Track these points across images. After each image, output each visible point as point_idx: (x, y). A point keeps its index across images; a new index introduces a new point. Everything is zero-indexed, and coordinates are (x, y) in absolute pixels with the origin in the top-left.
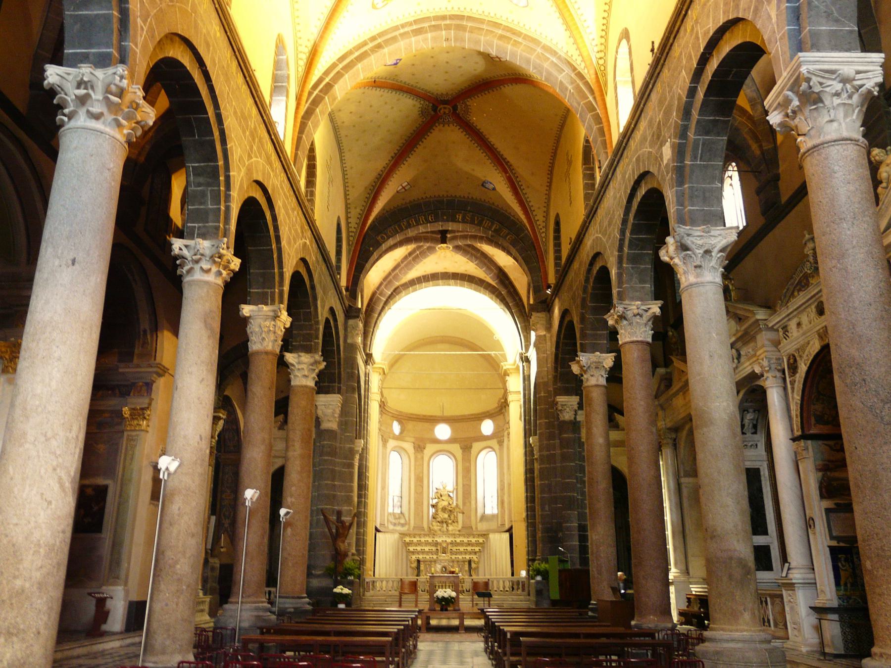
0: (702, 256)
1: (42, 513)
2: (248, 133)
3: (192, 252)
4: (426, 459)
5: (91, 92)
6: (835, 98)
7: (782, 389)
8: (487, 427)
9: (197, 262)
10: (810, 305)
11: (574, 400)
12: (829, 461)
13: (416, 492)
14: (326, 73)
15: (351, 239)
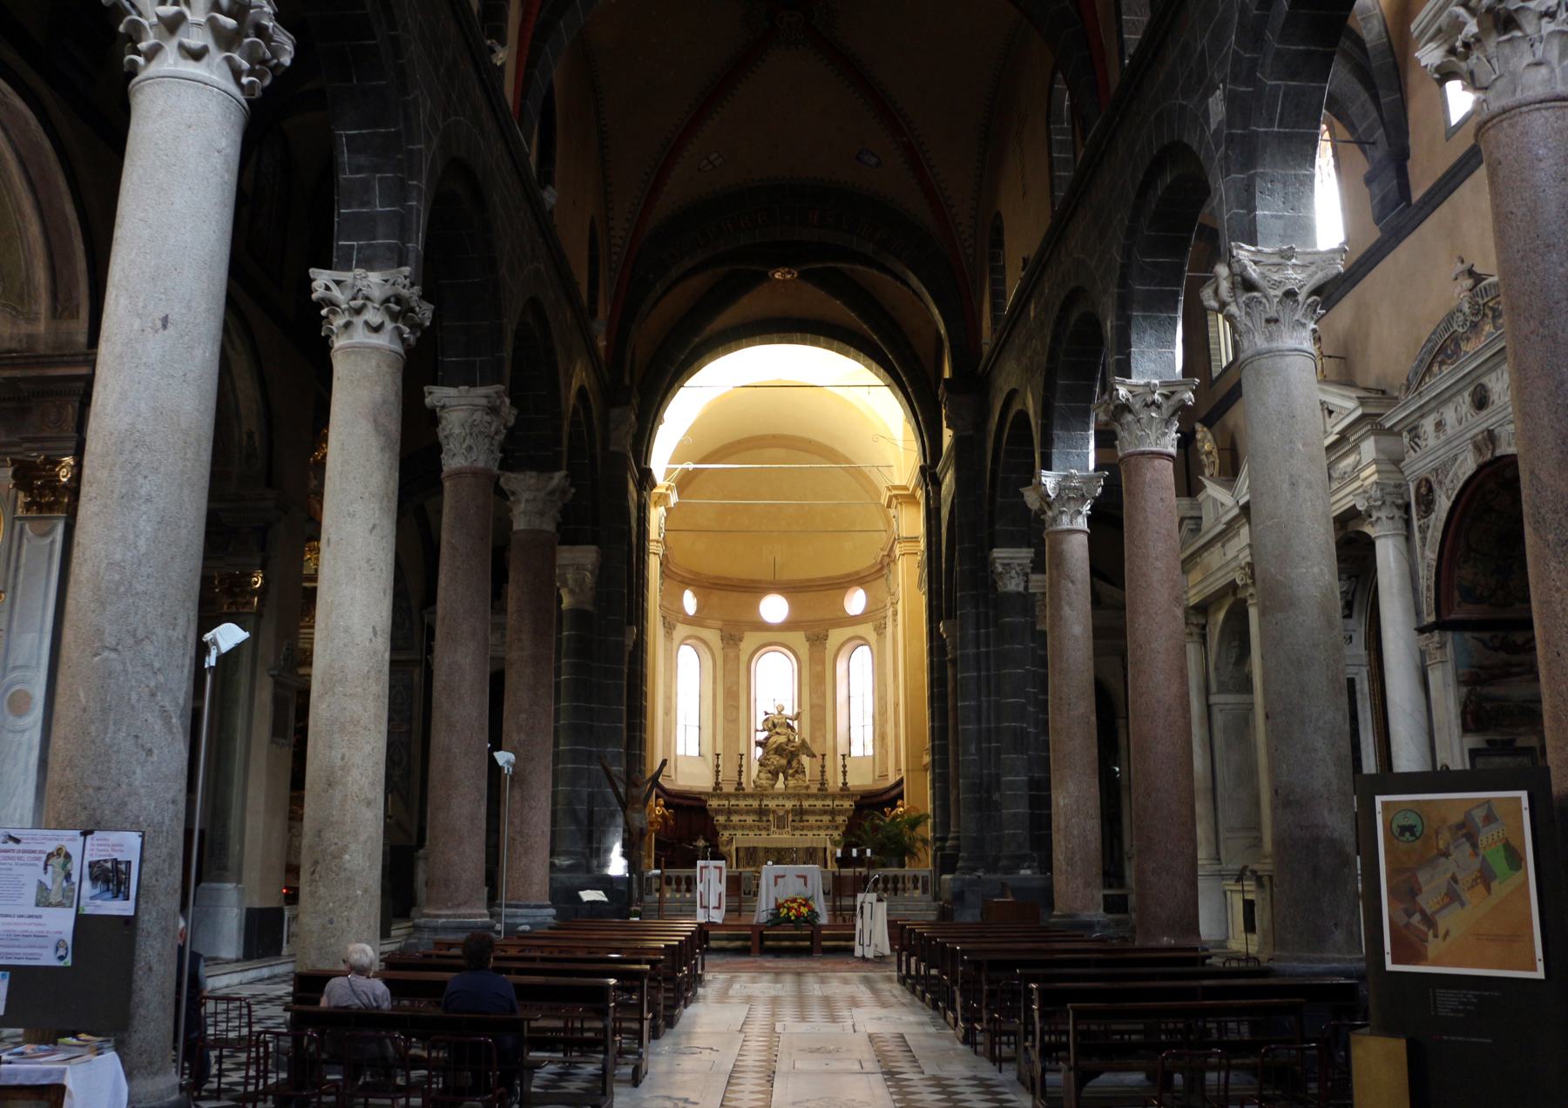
0: (1280, 302)
1: (138, 771)
3: (349, 294)
4: (744, 658)
5: (184, 9)
6: (1546, 20)
7: (1402, 540)
8: (856, 602)
9: (358, 311)
10: (1459, 392)
11: (1025, 554)
12: (1481, 667)
14: (989, 360)
15: (615, 258)
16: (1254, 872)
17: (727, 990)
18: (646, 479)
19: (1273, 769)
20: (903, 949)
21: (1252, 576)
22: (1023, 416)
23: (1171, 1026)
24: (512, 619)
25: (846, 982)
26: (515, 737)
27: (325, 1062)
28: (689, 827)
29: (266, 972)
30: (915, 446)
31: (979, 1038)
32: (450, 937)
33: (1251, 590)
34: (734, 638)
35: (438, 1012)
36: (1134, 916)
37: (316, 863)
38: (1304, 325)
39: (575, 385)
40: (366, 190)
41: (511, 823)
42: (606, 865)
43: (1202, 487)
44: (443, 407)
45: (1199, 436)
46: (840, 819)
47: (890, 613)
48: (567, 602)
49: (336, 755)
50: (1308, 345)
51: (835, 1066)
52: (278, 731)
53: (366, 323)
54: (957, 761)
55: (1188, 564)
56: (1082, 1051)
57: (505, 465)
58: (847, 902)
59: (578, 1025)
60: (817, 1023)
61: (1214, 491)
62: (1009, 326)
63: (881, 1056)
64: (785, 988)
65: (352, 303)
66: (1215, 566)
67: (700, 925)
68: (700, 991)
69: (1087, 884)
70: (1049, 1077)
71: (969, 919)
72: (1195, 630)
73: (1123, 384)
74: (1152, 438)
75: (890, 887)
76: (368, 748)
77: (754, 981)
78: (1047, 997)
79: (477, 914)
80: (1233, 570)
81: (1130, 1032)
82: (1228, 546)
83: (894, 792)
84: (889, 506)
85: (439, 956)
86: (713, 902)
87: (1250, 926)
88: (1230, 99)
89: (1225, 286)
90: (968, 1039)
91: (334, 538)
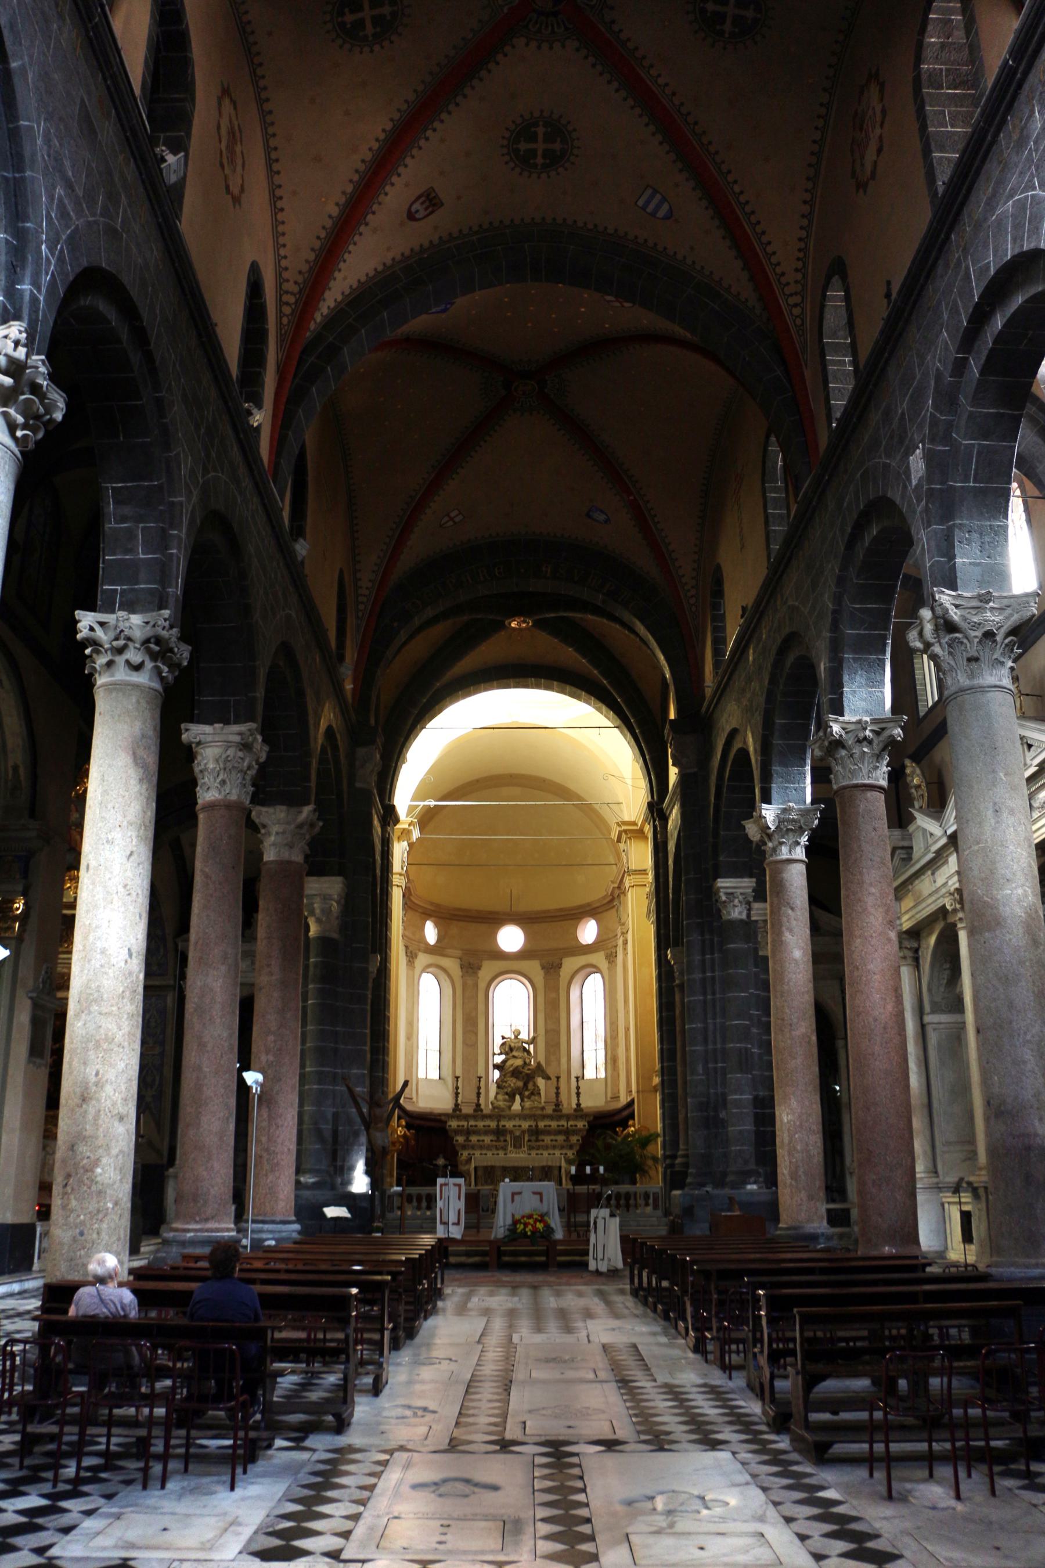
0: (980, 642)
2: (203, 430)
3: (112, 634)
4: (482, 985)
8: (588, 932)
9: (120, 651)
11: (747, 884)
13: (465, 1043)
15: (361, 607)
16: (969, 1184)
17: (466, 1303)
18: (390, 815)
19: (985, 1082)
20: (635, 1261)
21: (961, 901)
22: (744, 752)
23: (894, 1332)
24: (261, 945)
25: (580, 1294)
26: (263, 1058)
27: (71, 1372)
28: (427, 1147)
29: (16, 1287)
30: (643, 784)
31: (710, 1347)
32: (199, 1251)
33: (960, 915)
34: (472, 969)
35: (185, 1321)
36: (856, 1229)
37: (69, 1176)
38: (1002, 663)
39: (323, 725)
40: (131, 540)
41: (258, 1141)
42: (349, 1182)
43: (912, 819)
44: (199, 743)
45: (908, 771)
46: (574, 1139)
47: (620, 942)
48: (314, 930)
49: (90, 1071)
50: (1007, 682)
51: (571, 1374)
52: (35, 1050)
53: (127, 662)
54: (685, 1083)
55: (901, 891)
56: (809, 1356)
57: (255, 799)
58: (581, 1218)
59: (320, 1336)
60: (553, 1335)
61: (924, 822)
62: (728, 670)
63: (615, 1366)
64: (522, 1300)
65: (115, 643)
66: (926, 893)
67: (440, 1240)
68: (440, 1304)
69: (811, 1198)
70: (779, 1384)
71: (698, 1233)
72: (909, 954)
73: (836, 721)
74: (865, 771)
75: (622, 1204)
76: (121, 1065)
77: (491, 1294)
78: (773, 1303)
79: (225, 1229)
80: (943, 896)
81: (855, 1339)
82: (937, 873)
83: (625, 1113)
84: (619, 840)
85: (186, 1268)
86: (453, 1218)
87: (967, 1237)
88: (929, 457)
89: (928, 628)
90: (699, 1348)
91: (93, 864)
